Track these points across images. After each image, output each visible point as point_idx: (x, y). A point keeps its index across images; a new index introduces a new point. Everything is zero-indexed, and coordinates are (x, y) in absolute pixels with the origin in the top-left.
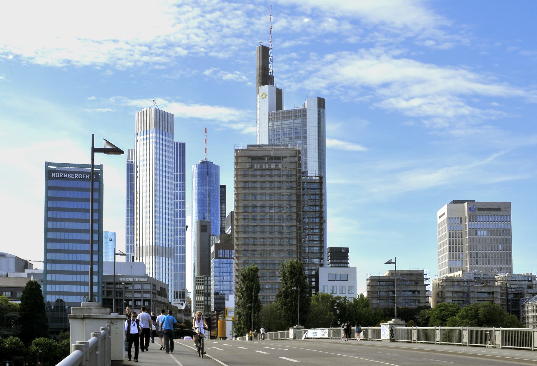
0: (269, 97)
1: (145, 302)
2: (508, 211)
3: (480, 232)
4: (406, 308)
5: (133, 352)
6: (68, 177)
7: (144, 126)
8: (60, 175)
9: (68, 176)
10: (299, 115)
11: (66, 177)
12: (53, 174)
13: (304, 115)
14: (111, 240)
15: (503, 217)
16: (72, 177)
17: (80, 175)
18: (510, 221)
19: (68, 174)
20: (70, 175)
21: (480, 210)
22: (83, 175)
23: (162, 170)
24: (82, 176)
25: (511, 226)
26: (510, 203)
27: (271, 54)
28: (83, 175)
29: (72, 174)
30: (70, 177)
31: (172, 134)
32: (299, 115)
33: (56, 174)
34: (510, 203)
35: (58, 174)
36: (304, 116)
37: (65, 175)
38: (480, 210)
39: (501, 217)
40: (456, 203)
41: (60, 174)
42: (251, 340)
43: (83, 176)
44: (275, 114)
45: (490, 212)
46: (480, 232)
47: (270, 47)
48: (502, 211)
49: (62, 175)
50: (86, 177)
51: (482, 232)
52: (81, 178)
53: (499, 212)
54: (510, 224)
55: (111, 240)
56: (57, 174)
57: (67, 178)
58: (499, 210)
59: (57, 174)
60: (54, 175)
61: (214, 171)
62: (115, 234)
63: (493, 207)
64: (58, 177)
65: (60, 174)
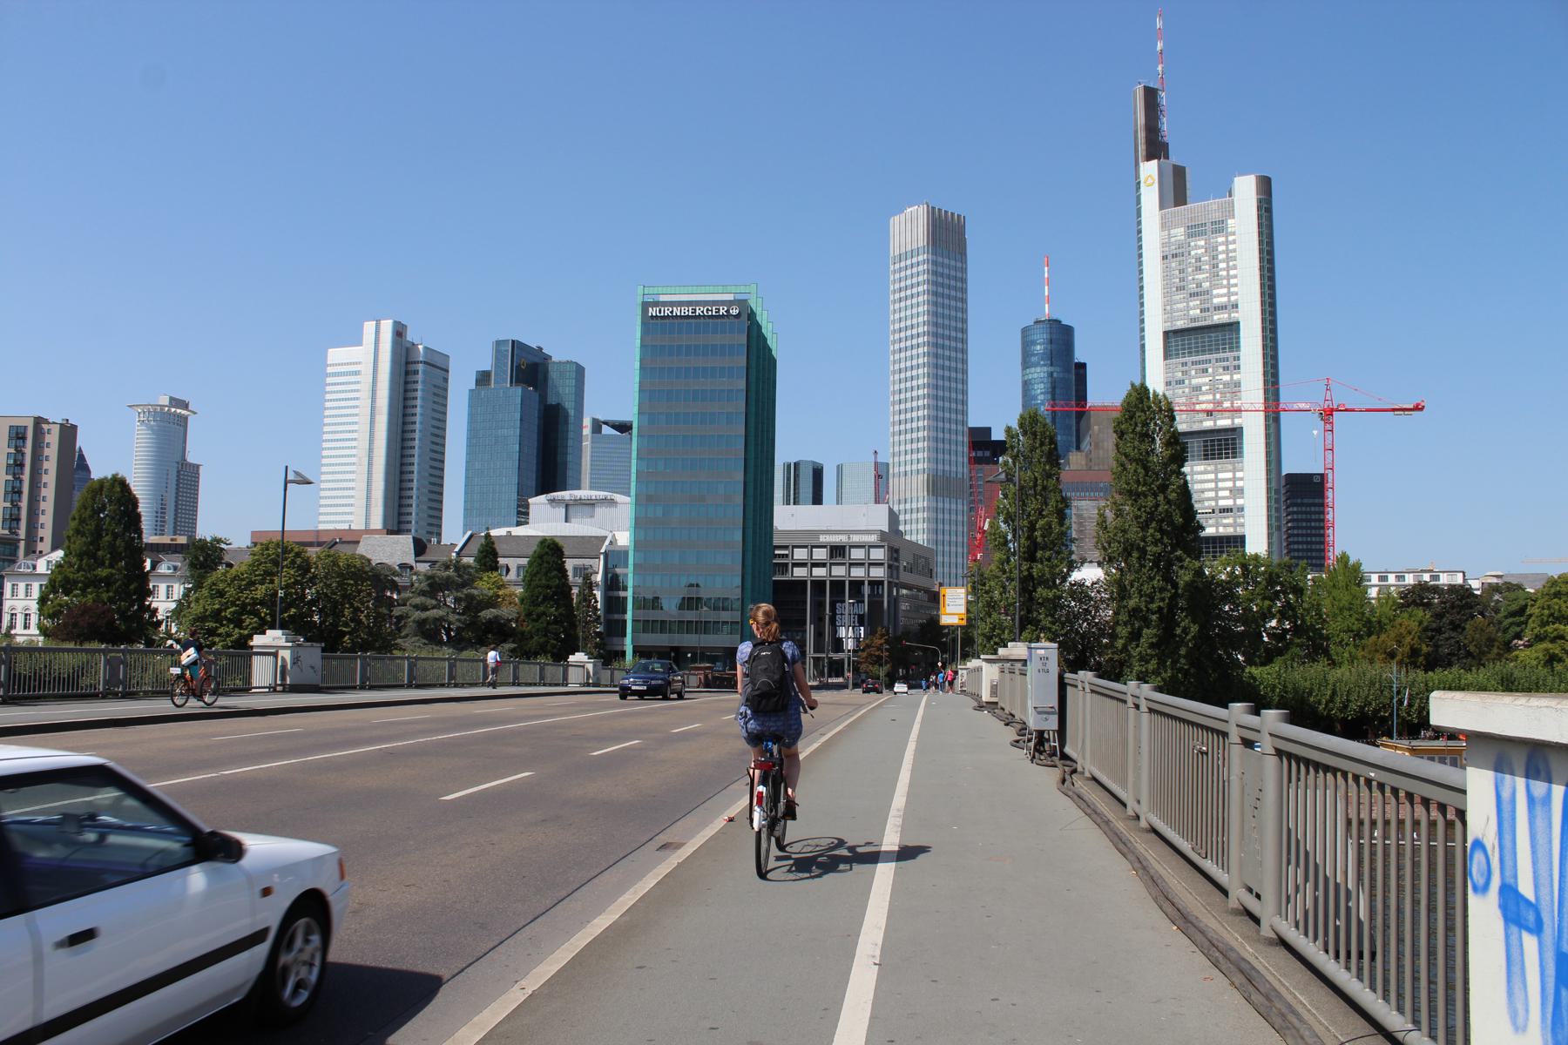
6: (683, 314)
11: (679, 314)
12: (650, 309)
16: (690, 314)
17: (708, 310)
19: (666, 309)
22: (714, 308)
24: (712, 311)
28: (714, 308)
29: (690, 308)
30: (687, 313)
35: (662, 309)
37: (677, 311)
41: (666, 309)
43: (690, 311)
49: (671, 309)
52: (710, 313)
57: (681, 316)
59: (660, 312)
64: (662, 314)
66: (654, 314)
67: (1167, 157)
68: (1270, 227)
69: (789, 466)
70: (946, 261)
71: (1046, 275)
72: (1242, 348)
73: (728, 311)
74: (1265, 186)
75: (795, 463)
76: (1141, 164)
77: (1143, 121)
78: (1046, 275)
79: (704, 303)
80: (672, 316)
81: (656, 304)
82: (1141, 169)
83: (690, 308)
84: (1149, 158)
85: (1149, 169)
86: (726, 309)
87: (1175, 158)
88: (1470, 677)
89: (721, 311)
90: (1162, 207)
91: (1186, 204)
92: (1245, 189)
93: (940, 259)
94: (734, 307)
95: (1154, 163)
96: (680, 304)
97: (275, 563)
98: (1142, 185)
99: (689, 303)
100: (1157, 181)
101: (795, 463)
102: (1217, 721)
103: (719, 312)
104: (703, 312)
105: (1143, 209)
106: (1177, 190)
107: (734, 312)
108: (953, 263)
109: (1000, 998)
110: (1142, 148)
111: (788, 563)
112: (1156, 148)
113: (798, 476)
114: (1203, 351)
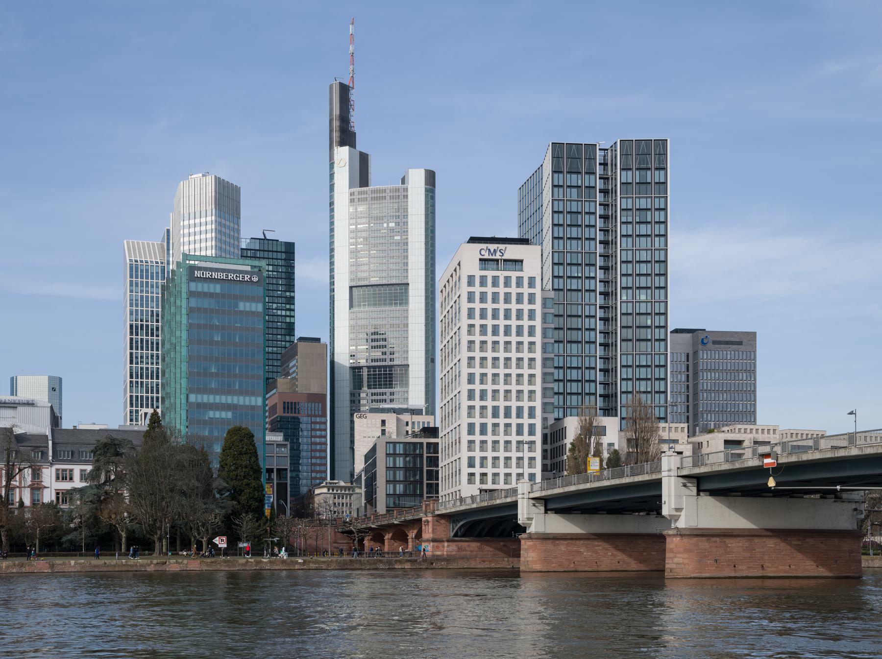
0: (349, 165)
1: (397, 459)
2: (752, 346)
5: (798, 458)
6: (219, 278)
7: (190, 205)
8: (208, 275)
9: (219, 275)
10: (396, 196)
11: (216, 277)
12: (196, 272)
13: (404, 196)
14: (55, 390)
16: (224, 278)
17: (236, 276)
19: (207, 273)
20: (233, 275)
21: (714, 343)
22: (241, 275)
24: (239, 277)
25: (755, 367)
26: (755, 334)
27: (354, 96)
28: (241, 275)
29: (224, 274)
30: (222, 278)
31: (239, 218)
32: (396, 196)
33: (201, 272)
34: (755, 334)
35: (205, 273)
36: (404, 198)
37: (215, 275)
38: (714, 343)
41: (207, 273)
43: (224, 276)
44: (360, 193)
47: (351, 85)
48: (745, 345)
49: (210, 274)
52: (238, 279)
53: (740, 346)
55: (55, 390)
56: (203, 273)
57: (218, 279)
58: (740, 343)
59: (203, 273)
60: (197, 274)
62: (60, 379)
64: (205, 276)
65: (219, 274)
66: (199, 276)
68: (433, 206)
70: (228, 223)
73: (250, 278)
74: (430, 178)
76: (335, 148)
77: (338, 113)
79: (234, 271)
82: (335, 152)
83: (224, 274)
84: (342, 143)
85: (342, 153)
86: (249, 277)
87: (361, 146)
89: (246, 278)
90: (351, 186)
91: (368, 186)
93: (223, 221)
98: (335, 165)
99: (223, 270)
100: (348, 164)
102: (776, 580)
103: (244, 279)
104: (233, 277)
105: (335, 186)
107: (255, 279)
108: (232, 225)
110: (336, 135)
111: (273, 469)
112: (347, 137)
114: (395, 304)
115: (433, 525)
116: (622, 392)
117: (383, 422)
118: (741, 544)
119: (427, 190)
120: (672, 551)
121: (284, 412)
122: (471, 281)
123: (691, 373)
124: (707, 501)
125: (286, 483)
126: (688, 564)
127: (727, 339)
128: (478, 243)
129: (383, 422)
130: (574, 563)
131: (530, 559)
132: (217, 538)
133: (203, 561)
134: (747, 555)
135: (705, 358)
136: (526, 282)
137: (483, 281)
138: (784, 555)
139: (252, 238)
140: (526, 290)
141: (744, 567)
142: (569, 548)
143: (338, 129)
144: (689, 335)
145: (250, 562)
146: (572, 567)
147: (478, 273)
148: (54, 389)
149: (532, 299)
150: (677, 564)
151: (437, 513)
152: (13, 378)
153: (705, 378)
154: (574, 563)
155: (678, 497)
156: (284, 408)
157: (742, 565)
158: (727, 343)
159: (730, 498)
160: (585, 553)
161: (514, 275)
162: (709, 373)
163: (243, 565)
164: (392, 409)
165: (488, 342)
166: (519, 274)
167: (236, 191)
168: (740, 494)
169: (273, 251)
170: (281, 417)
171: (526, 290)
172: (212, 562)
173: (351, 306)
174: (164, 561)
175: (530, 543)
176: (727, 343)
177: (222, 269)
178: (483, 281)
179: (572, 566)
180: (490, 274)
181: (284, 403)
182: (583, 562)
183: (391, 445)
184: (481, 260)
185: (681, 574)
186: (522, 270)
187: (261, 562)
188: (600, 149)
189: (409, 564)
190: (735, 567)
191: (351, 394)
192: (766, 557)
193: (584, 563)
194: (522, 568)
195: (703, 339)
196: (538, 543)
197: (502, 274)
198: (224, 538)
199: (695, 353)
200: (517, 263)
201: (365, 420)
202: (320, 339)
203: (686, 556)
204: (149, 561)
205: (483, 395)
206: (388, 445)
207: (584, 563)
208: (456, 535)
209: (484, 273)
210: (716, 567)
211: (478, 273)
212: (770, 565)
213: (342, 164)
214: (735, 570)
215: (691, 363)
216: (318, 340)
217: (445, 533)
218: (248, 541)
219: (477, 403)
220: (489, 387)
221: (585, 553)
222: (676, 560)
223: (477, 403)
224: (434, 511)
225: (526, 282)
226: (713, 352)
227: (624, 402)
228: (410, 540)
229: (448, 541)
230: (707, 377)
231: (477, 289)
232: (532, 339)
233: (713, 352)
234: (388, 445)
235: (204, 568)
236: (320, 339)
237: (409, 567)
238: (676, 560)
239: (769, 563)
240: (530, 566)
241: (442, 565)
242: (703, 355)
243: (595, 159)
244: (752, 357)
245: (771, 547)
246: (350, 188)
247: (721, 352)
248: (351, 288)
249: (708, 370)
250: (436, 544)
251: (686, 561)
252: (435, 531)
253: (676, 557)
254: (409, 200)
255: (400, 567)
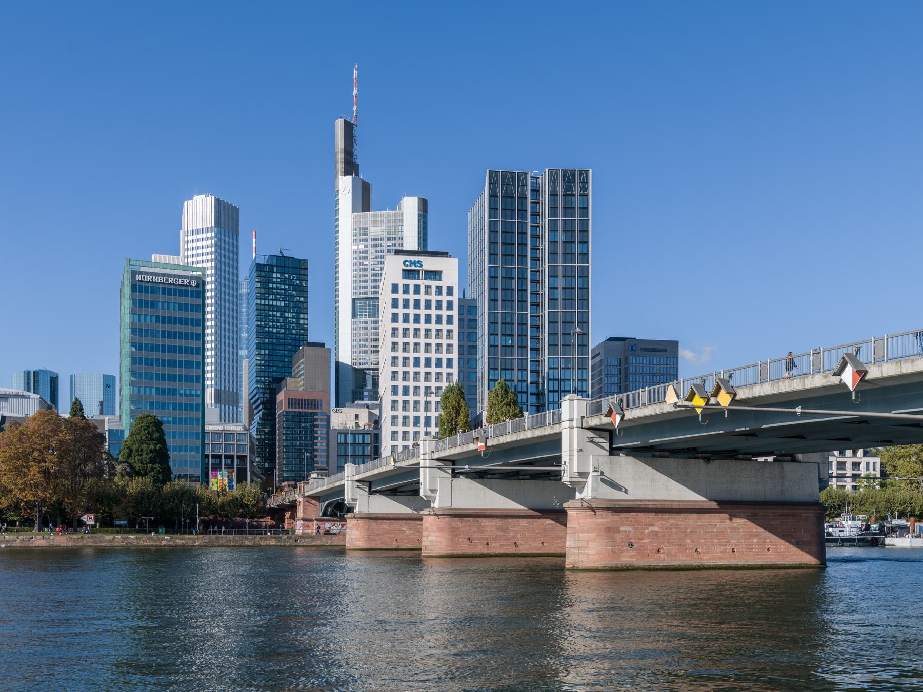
3: (611, 379)
4: (169, 458)
12: (137, 276)
15: (669, 359)
17: (176, 281)
18: (677, 365)
21: (643, 350)
23: (225, 284)
25: (677, 371)
26: (677, 342)
28: (180, 280)
29: (180, 280)
31: (238, 235)
34: (677, 342)
38: (643, 350)
39: (667, 359)
40: (614, 340)
42: (569, 178)
45: (654, 353)
46: (611, 379)
50: (184, 283)
51: (613, 378)
54: (677, 368)
56: (144, 277)
58: (665, 350)
59: (144, 277)
61: (491, 450)
63: (658, 347)
67: (357, 174)
69: (29, 373)
71: (254, 245)
72: (381, 314)
73: (189, 283)
74: (423, 206)
75: (34, 372)
77: (343, 146)
78: (254, 245)
79: (174, 276)
80: (153, 282)
81: (141, 273)
84: (347, 173)
86: (188, 281)
88: (694, 503)
90: (354, 210)
91: (369, 211)
92: (410, 205)
94: (194, 281)
95: (349, 178)
96: (158, 275)
97: (140, 430)
99: (163, 275)
100: (351, 191)
101: (34, 372)
106: (364, 201)
109: (893, 441)
112: (351, 168)
113: (38, 382)
115: (303, 506)
116: (549, 391)
117: (357, 416)
118: (493, 524)
119: (419, 216)
120: (427, 529)
121: (289, 407)
122: (395, 289)
123: (623, 376)
124: (463, 482)
125: (246, 469)
126: (441, 542)
127: (654, 347)
128: (407, 255)
129: (357, 416)
130: (396, 540)
131: (354, 537)
132: (85, 516)
133: (69, 537)
134: (500, 533)
135: (655, 363)
136: (444, 291)
137: (406, 289)
138: (537, 533)
139: (270, 255)
140: (444, 298)
141: (497, 545)
142: (391, 527)
143: (343, 161)
144: (621, 343)
145: (117, 538)
146: (394, 545)
147: (401, 282)
148: (108, 386)
149: (450, 306)
150: (432, 542)
151: (307, 494)
152: (72, 376)
153: (634, 380)
154: (396, 540)
155: (433, 479)
156: (289, 404)
157: (495, 543)
158: (654, 350)
159: (486, 480)
160: (407, 532)
161: (434, 284)
162: (648, 377)
163: (109, 541)
164: (366, 404)
165: (421, 344)
166: (438, 283)
167: (236, 211)
168: (528, 477)
169: (296, 268)
170: (286, 412)
171: (444, 298)
172: (79, 538)
173: (354, 315)
174: (31, 536)
175: (354, 522)
176: (654, 350)
177: (157, 273)
178: (406, 289)
179: (395, 543)
180: (412, 283)
181: (289, 399)
182: (405, 539)
183: (342, 435)
184: (403, 270)
185: (435, 552)
186: (440, 280)
187: (128, 538)
188: (531, 177)
189: (274, 540)
190: (488, 544)
191: (353, 392)
192: (519, 536)
193: (406, 541)
194: (348, 545)
195: (632, 347)
196: (361, 522)
197: (423, 283)
198: (92, 516)
199: (626, 359)
200: (435, 274)
201: (341, 414)
202: (324, 344)
203: (439, 534)
204: (15, 537)
205: (406, 391)
206: (339, 435)
207: (406, 541)
208: (324, 514)
209: (407, 282)
210: (469, 545)
211: (401, 282)
212: (523, 543)
213: (346, 192)
214: (488, 548)
215: (622, 367)
216: (322, 345)
217: (315, 513)
218: (125, 520)
219: (400, 398)
220: (411, 384)
221: (407, 532)
222: (430, 538)
223: (400, 398)
224: (304, 492)
225: (444, 291)
226: (641, 358)
227: (551, 400)
228: (286, 520)
229: (317, 520)
230: (636, 380)
231: (401, 296)
232: (449, 342)
233: (641, 358)
234: (339, 435)
235: (70, 544)
236: (324, 344)
237: (274, 544)
238: (430, 538)
239: (521, 540)
240: (354, 543)
241: (306, 542)
242: (633, 360)
243: (527, 186)
244: (675, 362)
245: (525, 526)
246: (353, 212)
247: (648, 358)
248: (354, 300)
249: (636, 374)
250: (306, 523)
251: (439, 539)
252: (305, 511)
253: (430, 535)
254: (404, 224)
255: (265, 544)
